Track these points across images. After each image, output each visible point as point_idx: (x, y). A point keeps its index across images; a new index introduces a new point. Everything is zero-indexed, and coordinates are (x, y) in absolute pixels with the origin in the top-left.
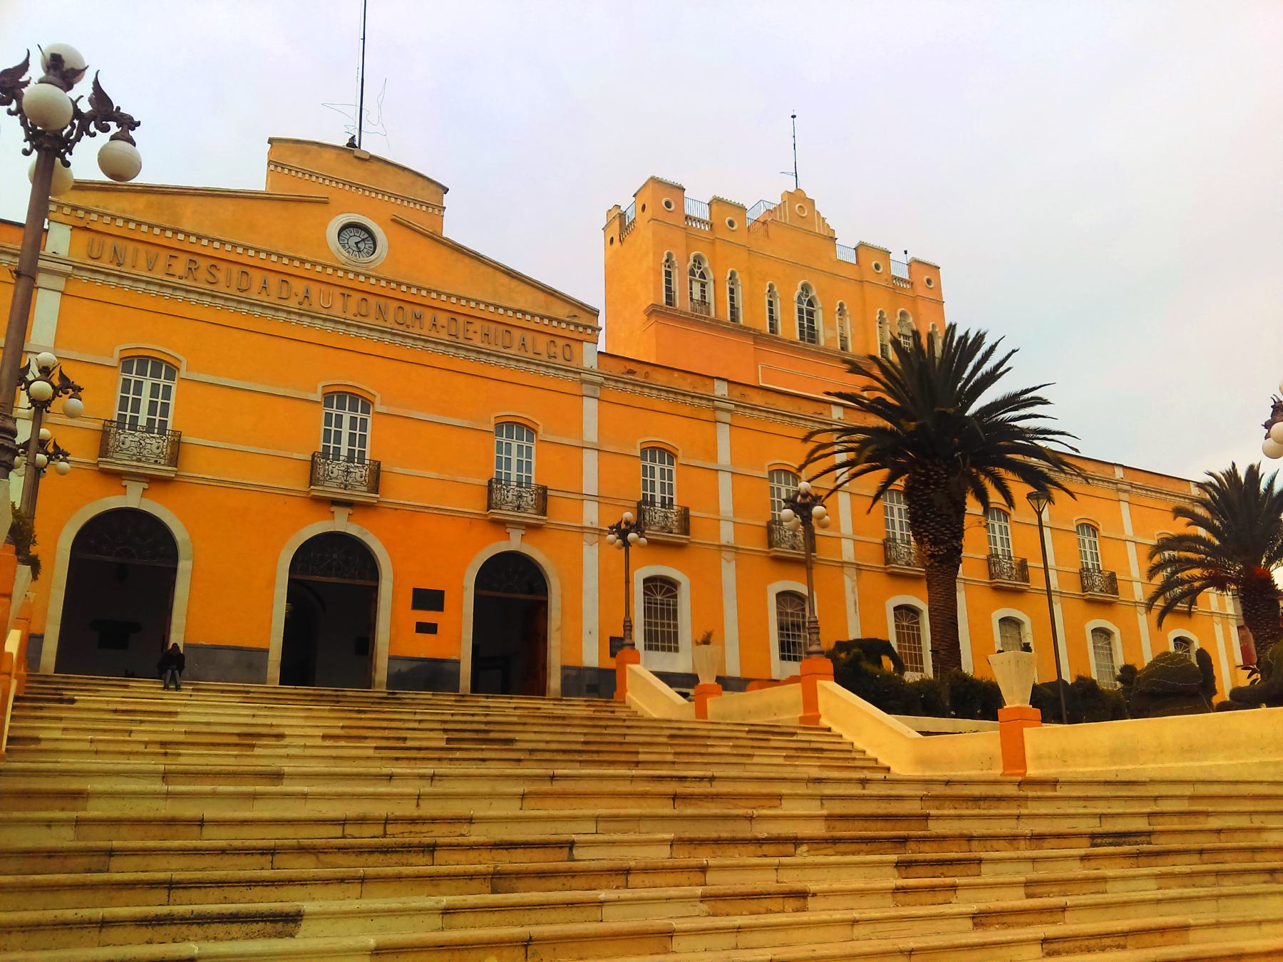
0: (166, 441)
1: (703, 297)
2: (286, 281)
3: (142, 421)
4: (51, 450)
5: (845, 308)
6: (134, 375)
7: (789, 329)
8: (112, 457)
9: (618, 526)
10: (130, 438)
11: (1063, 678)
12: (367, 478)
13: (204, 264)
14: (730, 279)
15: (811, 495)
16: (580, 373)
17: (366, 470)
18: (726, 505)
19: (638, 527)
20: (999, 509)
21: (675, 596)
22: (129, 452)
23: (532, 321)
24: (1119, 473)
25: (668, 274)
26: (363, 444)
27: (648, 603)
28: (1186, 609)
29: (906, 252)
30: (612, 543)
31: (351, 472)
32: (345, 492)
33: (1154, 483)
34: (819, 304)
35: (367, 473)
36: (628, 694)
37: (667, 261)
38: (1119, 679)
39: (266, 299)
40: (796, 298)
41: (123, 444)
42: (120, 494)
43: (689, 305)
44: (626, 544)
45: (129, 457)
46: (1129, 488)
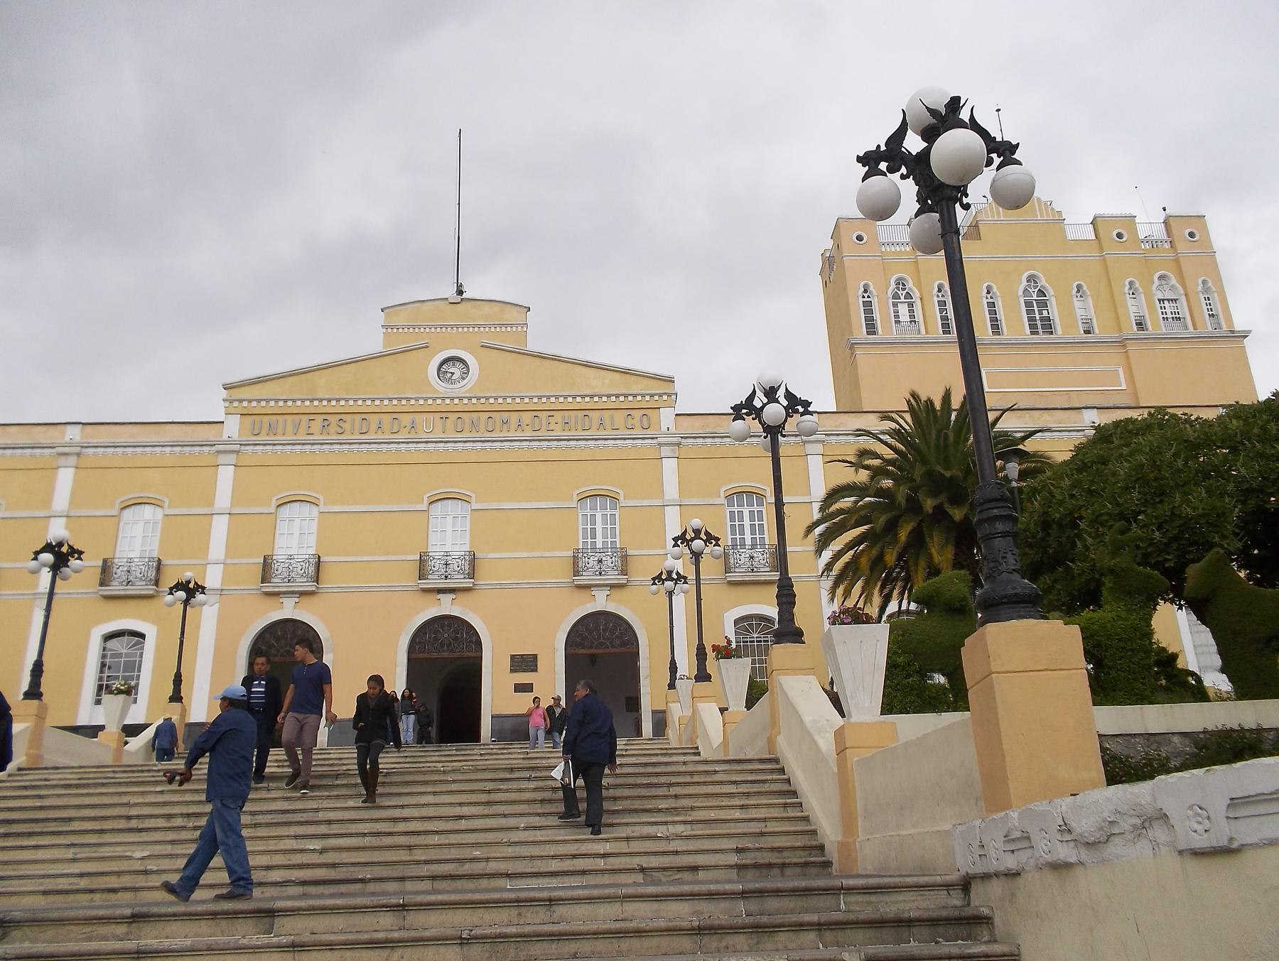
1: (912, 316)
3: (748, 542)
4: (675, 576)
6: (589, 511)
16: (657, 438)
21: (142, 648)
26: (762, 532)
32: (600, 577)
34: (1050, 292)
40: (1021, 293)
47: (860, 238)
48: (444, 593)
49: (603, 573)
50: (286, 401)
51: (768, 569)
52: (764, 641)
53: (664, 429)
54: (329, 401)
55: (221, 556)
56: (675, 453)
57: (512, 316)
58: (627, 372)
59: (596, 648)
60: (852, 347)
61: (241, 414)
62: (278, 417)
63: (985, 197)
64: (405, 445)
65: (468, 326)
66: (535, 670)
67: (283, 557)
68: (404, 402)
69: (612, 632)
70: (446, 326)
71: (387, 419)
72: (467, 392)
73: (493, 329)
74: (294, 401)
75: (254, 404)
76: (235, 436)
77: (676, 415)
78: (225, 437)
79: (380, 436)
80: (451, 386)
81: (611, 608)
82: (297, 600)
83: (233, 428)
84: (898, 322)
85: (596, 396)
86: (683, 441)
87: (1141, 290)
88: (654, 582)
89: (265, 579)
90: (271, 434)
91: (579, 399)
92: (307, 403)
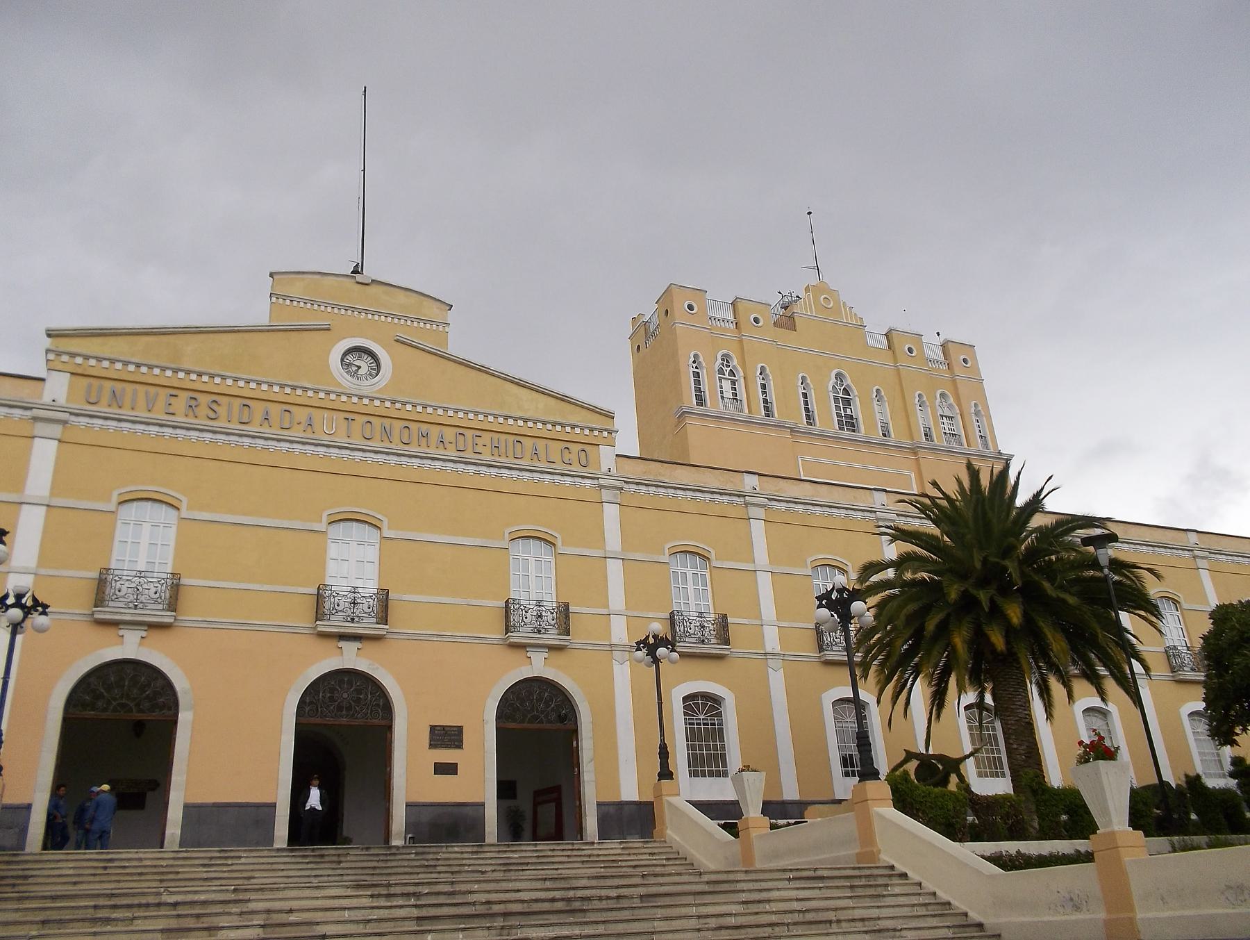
0: (165, 585)
2: (195, 399)
5: (883, 394)
7: (827, 420)
8: (108, 606)
9: (645, 642)
10: (127, 584)
11: (1164, 780)
12: (375, 609)
13: (204, 400)
14: (761, 374)
15: (848, 590)
16: (598, 478)
17: (557, 613)
18: (768, 608)
19: (669, 643)
20: (1168, 597)
22: (125, 600)
23: (544, 430)
24: (1193, 538)
25: (697, 375)
27: (690, 724)
28: (1203, 678)
29: (938, 334)
30: (640, 661)
31: (358, 603)
32: (352, 625)
33: (1148, 536)
34: (855, 392)
35: (375, 603)
36: (669, 832)
37: (694, 362)
38: (1232, 775)
39: (268, 430)
40: (830, 388)
41: (119, 591)
42: (117, 644)
43: (721, 404)
44: (656, 661)
45: (126, 604)
46: (1207, 554)
47: (690, 307)
48: (347, 640)
49: (357, 619)
50: (138, 365)
51: (694, 640)
52: (697, 724)
53: (604, 469)
54: (200, 375)
55: (32, 563)
56: (617, 498)
57: (432, 311)
58: (564, 399)
59: (528, 723)
60: (683, 415)
61: (72, 374)
62: (158, 389)
63: (780, 293)
64: (300, 446)
65: (380, 314)
66: (460, 746)
67: (345, 589)
68: (299, 392)
69: (547, 704)
70: (353, 309)
71: (275, 410)
72: (378, 391)
73: (409, 323)
74: (150, 367)
75: (93, 362)
76: (62, 400)
77: (617, 455)
78: (47, 399)
79: (265, 429)
80: (358, 382)
81: (549, 674)
82: (144, 634)
83: (57, 389)
84: (723, 398)
85: (530, 420)
86: (626, 486)
87: (928, 404)
88: (638, 647)
89: (100, 600)
90: (115, 405)
91: (511, 421)
92: (169, 373)
